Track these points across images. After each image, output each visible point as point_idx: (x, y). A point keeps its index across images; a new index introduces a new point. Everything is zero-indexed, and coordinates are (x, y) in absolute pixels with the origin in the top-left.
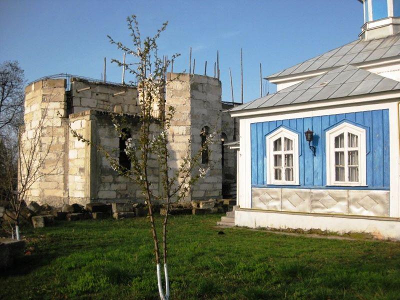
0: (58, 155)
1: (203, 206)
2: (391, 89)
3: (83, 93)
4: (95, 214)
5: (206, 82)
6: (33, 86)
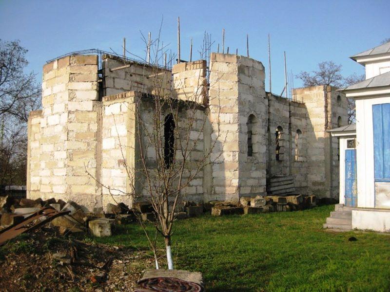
0: (89, 145)
1: (256, 204)
2: (365, 87)
3: (117, 73)
4: (146, 215)
5: (251, 66)
6: (55, 64)
